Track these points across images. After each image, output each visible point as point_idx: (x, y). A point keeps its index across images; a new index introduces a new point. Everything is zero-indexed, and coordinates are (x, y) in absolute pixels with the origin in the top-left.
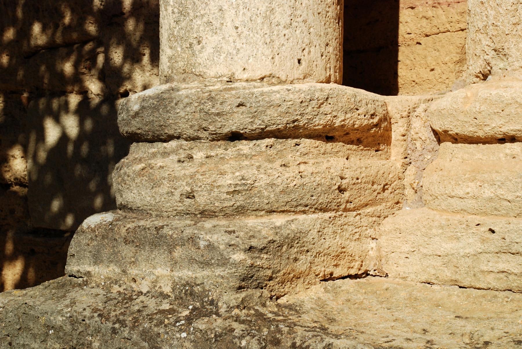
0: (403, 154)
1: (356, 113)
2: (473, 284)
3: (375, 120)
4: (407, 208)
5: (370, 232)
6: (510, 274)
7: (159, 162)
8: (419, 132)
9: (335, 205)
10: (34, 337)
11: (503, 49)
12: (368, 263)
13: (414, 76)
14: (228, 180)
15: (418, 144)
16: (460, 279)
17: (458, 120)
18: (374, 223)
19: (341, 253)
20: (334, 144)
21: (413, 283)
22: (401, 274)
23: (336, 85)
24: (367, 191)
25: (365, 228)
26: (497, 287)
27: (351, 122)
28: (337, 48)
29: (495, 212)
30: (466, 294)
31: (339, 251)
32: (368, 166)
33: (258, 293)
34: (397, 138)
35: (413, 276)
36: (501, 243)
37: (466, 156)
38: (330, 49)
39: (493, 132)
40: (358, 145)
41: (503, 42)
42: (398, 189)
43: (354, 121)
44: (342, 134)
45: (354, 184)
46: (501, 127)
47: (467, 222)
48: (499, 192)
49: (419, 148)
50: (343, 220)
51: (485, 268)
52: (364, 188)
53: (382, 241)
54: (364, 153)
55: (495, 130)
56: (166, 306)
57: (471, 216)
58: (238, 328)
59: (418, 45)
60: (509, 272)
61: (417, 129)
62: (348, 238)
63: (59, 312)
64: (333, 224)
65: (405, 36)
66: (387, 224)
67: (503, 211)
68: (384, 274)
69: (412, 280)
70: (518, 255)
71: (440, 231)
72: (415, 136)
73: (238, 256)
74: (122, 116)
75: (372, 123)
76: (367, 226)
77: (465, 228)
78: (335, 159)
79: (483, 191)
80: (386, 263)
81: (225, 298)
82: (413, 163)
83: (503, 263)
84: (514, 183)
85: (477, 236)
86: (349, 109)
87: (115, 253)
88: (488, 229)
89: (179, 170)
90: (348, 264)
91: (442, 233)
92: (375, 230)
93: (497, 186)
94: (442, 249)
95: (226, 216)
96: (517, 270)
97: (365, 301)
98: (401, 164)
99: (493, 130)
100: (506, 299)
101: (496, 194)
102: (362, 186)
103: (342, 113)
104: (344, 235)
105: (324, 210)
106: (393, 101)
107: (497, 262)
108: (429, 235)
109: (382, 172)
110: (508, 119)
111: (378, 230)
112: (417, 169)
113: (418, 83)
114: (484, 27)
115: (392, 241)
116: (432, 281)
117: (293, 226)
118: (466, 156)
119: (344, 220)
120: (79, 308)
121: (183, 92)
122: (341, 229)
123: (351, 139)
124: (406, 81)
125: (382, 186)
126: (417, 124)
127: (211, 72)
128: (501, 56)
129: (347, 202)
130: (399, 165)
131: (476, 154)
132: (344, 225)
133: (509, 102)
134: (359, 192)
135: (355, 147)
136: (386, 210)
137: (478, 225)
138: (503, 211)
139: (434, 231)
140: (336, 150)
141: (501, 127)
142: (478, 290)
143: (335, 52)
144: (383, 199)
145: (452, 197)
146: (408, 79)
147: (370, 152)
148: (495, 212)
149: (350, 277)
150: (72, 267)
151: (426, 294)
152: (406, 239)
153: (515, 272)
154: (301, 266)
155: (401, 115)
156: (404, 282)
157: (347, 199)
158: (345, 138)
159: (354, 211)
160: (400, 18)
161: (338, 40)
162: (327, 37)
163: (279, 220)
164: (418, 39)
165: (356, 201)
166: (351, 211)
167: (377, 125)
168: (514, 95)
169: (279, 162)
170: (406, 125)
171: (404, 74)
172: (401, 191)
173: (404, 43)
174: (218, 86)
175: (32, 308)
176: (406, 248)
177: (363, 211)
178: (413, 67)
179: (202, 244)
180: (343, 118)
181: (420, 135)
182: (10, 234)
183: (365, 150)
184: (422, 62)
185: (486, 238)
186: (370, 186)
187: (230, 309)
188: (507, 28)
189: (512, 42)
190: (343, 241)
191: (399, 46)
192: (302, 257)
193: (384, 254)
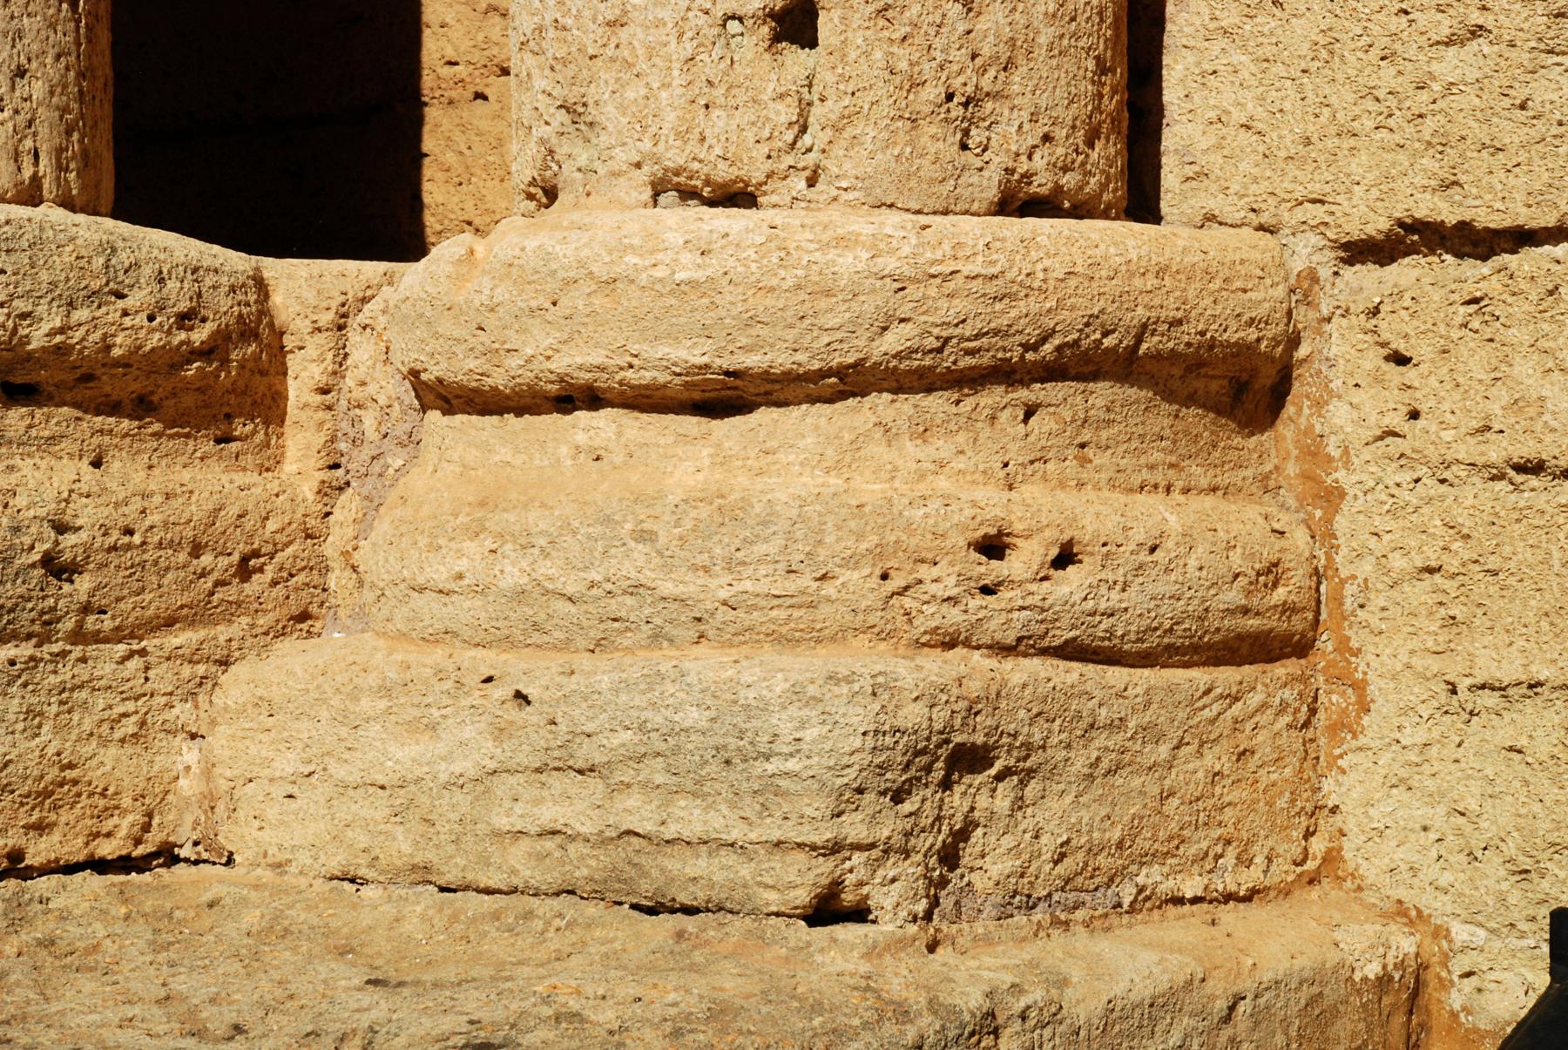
0: (323, 454)
1: (112, 307)
2: (470, 877)
3: (200, 335)
4: (336, 635)
6: (572, 838)
8: (368, 380)
9: (33, 621)
11: (584, 105)
12: (171, 817)
13: (469, 205)
15: (369, 420)
16: (435, 860)
17: (437, 335)
18: (201, 684)
19: (61, 785)
20: (38, 413)
21: (303, 882)
22: (270, 852)
23: (58, 215)
24: (170, 576)
25: (163, 700)
26: (536, 885)
27: (96, 336)
28: (65, 87)
29: (536, 638)
30: (449, 912)
31: (48, 778)
32: (179, 491)
34: (304, 400)
35: (304, 858)
36: (541, 738)
37: (472, 455)
39: (529, 374)
40: (140, 419)
41: (585, 84)
42: (303, 569)
43: (105, 337)
44: (70, 377)
45: (113, 548)
46: (548, 358)
47: (459, 673)
48: (543, 570)
49: (371, 434)
51: (505, 820)
52: (156, 563)
53: (219, 741)
54: (167, 445)
55: (540, 365)
57: (474, 652)
59: (479, 101)
60: (569, 832)
61: (363, 369)
62: (91, 734)
64: (25, 685)
65: (439, 70)
66: (236, 686)
67: (557, 634)
68: (221, 856)
69: (301, 873)
70: (593, 774)
71: (383, 704)
72: (358, 394)
75: (188, 342)
76: (171, 694)
77: (452, 691)
78: (43, 464)
79: (499, 567)
80: (229, 818)
82: (353, 484)
83: (555, 803)
84: (584, 540)
85: (483, 718)
86: (83, 293)
88: (513, 693)
90: (89, 822)
91: (388, 712)
92: (197, 707)
93: (536, 551)
94: (390, 763)
96: (589, 823)
97: (108, 942)
98: (315, 485)
99: (531, 367)
100: (557, 922)
101: (534, 575)
102: (145, 557)
103: (55, 304)
104: (75, 722)
106: (290, 277)
107: (538, 802)
108: (352, 716)
109: (234, 511)
110: (567, 329)
111: (207, 706)
112: (366, 503)
113: (481, 228)
114: (537, 32)
115: (247, 742)
116: (360, 873)
118: (472, 455)
119: (76, 671)
122: (61, 703)
123: (108, 396)
124: (446, 222)
125: (236, 558)
126: (362, 350)
128: (582, 127)
129: (86, 609)
130: (308, 490)
131: (497, 448)
132: (72, 690)
133: (572, 274)
134: (136, 577)
135: (126, 424)
136: (251, 640)
137: (489, 680)
138: (557, 634)
139: (365, 703)
140: (47, 433)
141: (548, 358)
142: (486, 897)
143: (55, 100)
144: (239, 604)
145: (421, 590)
146: (453, 217)
147: (191, 442)
149: (100, 866)
151: (330, 915)
152: (285, 734)
153: (583, 830)
155: (315, 322)
156: (278, 880)
157: (84, 598)
158: (83, 393)
159: (120, 642)
160: (424, 9)
161: (72, 59)
162: (19, 46)
164: (478, 80)
165: (125, 606)
166: (106, 641)
167: (206, 352)
168: (585, 252)
170: (330, 356)
171: (440, 199)
172: (315, 577)
173: (437, 95)
176: (288, 763)
177: (156, 642)
178: (466, 176)
180: (58, 323)
181: (372, 389)
183: (171, 437)
184: (491, 159)
185: (507, 721)
186: (182, 557)
188: (591, 36)
189: (606, 82)
190: (68, 745)
191: (426, 104)
193: (224, 785)
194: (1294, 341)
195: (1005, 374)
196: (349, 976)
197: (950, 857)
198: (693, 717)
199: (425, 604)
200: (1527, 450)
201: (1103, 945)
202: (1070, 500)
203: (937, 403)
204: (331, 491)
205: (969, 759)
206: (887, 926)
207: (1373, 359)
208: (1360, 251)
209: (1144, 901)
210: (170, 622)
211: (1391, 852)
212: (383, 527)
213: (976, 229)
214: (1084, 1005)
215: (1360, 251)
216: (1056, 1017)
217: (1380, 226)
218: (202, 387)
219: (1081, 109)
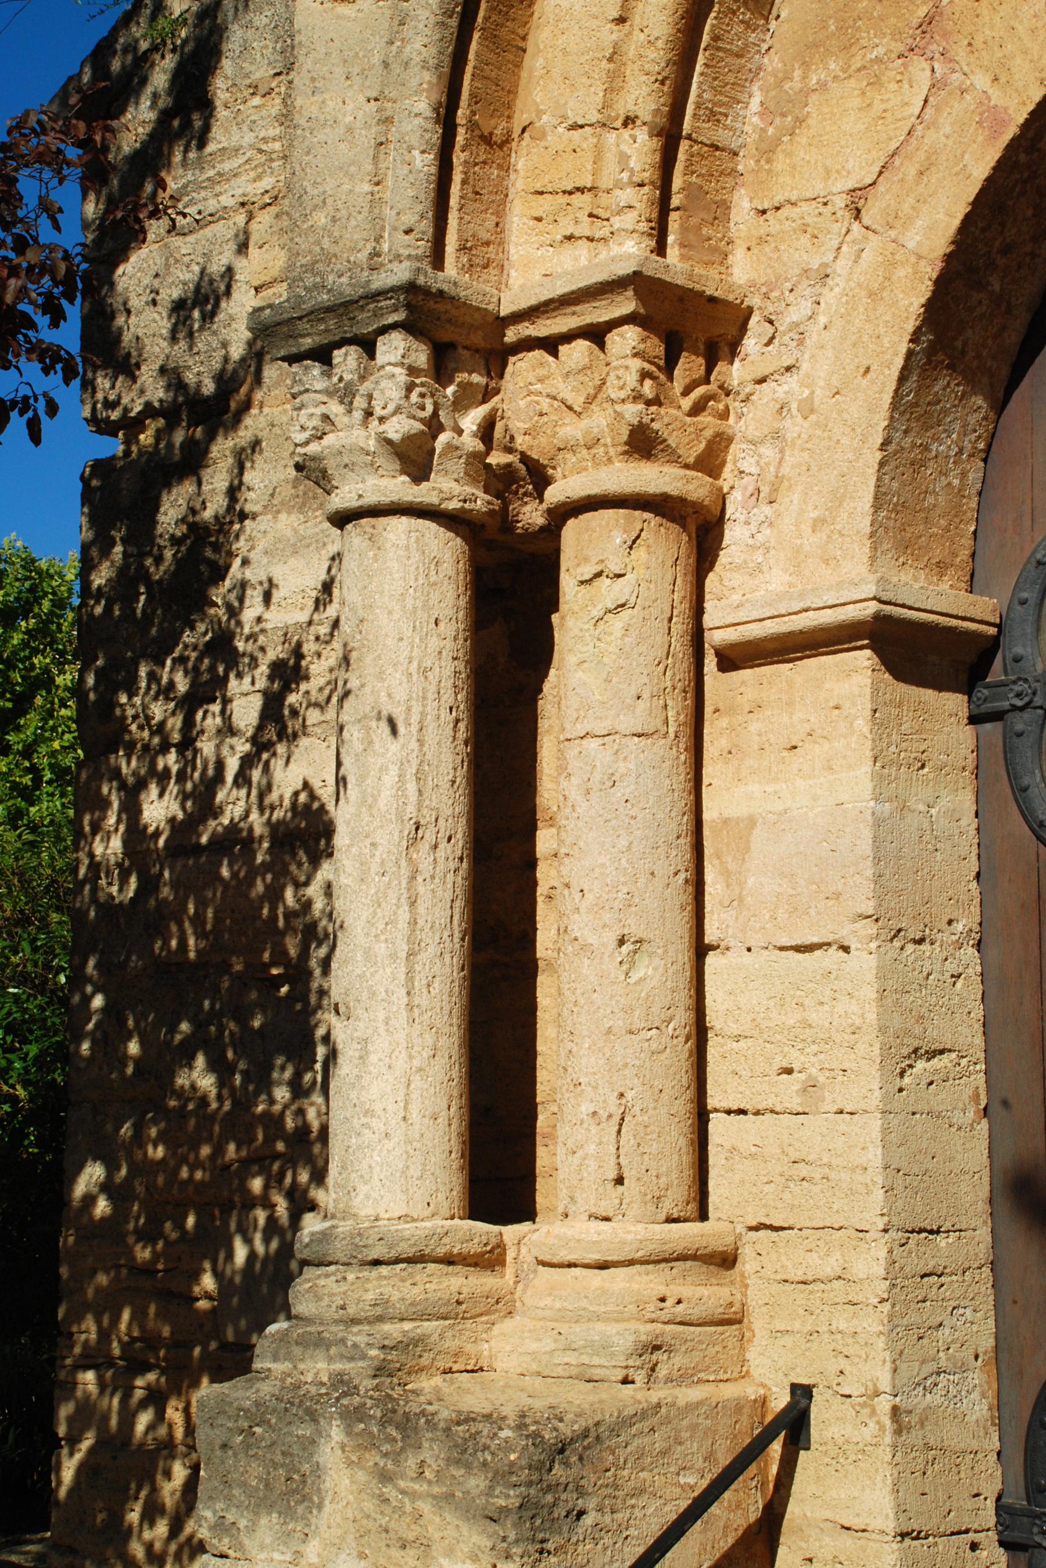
3: (488, 1248)
5: (484, 1336)
7: (322, 1282)
10: (229, 1418)
14: (370, 1296)
33: (389, 1380)
38: (455, 1193)
50: (461, 1327)
53: (493, 1343)
56: (323, 1391)
58: (369, 1403)
63: (248, 1398)
66: (496, 1330)
73: (374, 1352)
74: (297, 1246)
81: (364, 1383)
87: (289, 1353)
89: (336, 1288)
95: (370, 1323)
105: (445, 1318)
117: (418, 1331)
120: (262, 1394)
121: (340, 1230)
126: (524, 1250)
127: (363, 1213)
130: (511, 1283)
148: (561, 1319)
149: (468, 1371)
150: (257, 1365)
154: (425, 1361)
163: (407, 1326)
167: (490, 1252)
169: (410, 1281)
174: (366, 1224)
175: (228, 1396)
176: (508, 1348)
179: (349, 1343)
182: (63, 1492)
187: (367, 1391)
192: (426, 1355)
194: (737, 1249)
195: (666, 1260)
196: (524, 1395)
197: (653, 1370)
198: (597, 1338)
199: (538, 1311)
200: (784, 1277)
201: (689, 1391)
202: (680, 1288)
203: (650, 1267)
204: (517, 1283)
205: (657, 1348)
206: (638, 1385)
207: (754, 1254)
208: (751, 1229)
209: (700, 1381)
210: (481, 1315)
211: (760, 1371)
212: (529, 1293)
213: (657, 1227)
214: (681, 1402)
215: (751, 1229)
216: (674, 1404)
217: (754, 1224)
218: (489, 1259)
219: (685, 1197)
